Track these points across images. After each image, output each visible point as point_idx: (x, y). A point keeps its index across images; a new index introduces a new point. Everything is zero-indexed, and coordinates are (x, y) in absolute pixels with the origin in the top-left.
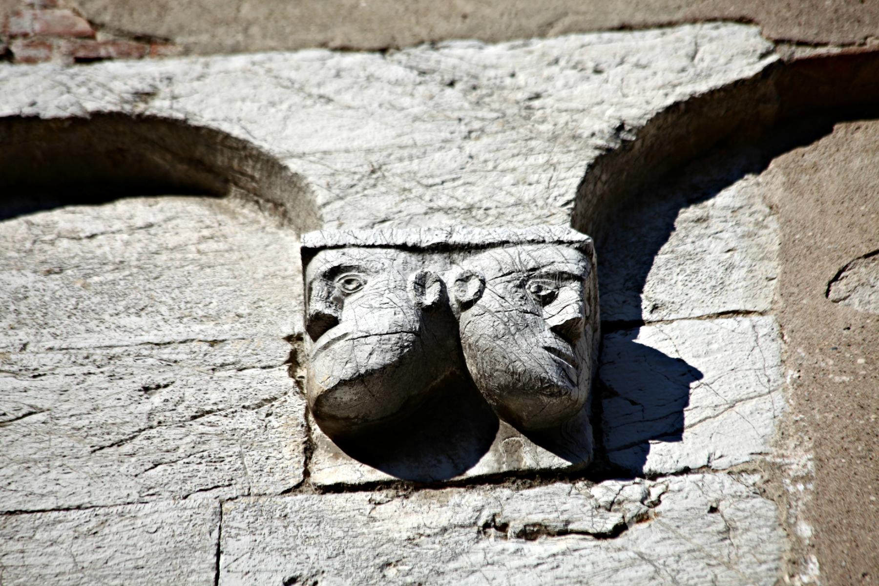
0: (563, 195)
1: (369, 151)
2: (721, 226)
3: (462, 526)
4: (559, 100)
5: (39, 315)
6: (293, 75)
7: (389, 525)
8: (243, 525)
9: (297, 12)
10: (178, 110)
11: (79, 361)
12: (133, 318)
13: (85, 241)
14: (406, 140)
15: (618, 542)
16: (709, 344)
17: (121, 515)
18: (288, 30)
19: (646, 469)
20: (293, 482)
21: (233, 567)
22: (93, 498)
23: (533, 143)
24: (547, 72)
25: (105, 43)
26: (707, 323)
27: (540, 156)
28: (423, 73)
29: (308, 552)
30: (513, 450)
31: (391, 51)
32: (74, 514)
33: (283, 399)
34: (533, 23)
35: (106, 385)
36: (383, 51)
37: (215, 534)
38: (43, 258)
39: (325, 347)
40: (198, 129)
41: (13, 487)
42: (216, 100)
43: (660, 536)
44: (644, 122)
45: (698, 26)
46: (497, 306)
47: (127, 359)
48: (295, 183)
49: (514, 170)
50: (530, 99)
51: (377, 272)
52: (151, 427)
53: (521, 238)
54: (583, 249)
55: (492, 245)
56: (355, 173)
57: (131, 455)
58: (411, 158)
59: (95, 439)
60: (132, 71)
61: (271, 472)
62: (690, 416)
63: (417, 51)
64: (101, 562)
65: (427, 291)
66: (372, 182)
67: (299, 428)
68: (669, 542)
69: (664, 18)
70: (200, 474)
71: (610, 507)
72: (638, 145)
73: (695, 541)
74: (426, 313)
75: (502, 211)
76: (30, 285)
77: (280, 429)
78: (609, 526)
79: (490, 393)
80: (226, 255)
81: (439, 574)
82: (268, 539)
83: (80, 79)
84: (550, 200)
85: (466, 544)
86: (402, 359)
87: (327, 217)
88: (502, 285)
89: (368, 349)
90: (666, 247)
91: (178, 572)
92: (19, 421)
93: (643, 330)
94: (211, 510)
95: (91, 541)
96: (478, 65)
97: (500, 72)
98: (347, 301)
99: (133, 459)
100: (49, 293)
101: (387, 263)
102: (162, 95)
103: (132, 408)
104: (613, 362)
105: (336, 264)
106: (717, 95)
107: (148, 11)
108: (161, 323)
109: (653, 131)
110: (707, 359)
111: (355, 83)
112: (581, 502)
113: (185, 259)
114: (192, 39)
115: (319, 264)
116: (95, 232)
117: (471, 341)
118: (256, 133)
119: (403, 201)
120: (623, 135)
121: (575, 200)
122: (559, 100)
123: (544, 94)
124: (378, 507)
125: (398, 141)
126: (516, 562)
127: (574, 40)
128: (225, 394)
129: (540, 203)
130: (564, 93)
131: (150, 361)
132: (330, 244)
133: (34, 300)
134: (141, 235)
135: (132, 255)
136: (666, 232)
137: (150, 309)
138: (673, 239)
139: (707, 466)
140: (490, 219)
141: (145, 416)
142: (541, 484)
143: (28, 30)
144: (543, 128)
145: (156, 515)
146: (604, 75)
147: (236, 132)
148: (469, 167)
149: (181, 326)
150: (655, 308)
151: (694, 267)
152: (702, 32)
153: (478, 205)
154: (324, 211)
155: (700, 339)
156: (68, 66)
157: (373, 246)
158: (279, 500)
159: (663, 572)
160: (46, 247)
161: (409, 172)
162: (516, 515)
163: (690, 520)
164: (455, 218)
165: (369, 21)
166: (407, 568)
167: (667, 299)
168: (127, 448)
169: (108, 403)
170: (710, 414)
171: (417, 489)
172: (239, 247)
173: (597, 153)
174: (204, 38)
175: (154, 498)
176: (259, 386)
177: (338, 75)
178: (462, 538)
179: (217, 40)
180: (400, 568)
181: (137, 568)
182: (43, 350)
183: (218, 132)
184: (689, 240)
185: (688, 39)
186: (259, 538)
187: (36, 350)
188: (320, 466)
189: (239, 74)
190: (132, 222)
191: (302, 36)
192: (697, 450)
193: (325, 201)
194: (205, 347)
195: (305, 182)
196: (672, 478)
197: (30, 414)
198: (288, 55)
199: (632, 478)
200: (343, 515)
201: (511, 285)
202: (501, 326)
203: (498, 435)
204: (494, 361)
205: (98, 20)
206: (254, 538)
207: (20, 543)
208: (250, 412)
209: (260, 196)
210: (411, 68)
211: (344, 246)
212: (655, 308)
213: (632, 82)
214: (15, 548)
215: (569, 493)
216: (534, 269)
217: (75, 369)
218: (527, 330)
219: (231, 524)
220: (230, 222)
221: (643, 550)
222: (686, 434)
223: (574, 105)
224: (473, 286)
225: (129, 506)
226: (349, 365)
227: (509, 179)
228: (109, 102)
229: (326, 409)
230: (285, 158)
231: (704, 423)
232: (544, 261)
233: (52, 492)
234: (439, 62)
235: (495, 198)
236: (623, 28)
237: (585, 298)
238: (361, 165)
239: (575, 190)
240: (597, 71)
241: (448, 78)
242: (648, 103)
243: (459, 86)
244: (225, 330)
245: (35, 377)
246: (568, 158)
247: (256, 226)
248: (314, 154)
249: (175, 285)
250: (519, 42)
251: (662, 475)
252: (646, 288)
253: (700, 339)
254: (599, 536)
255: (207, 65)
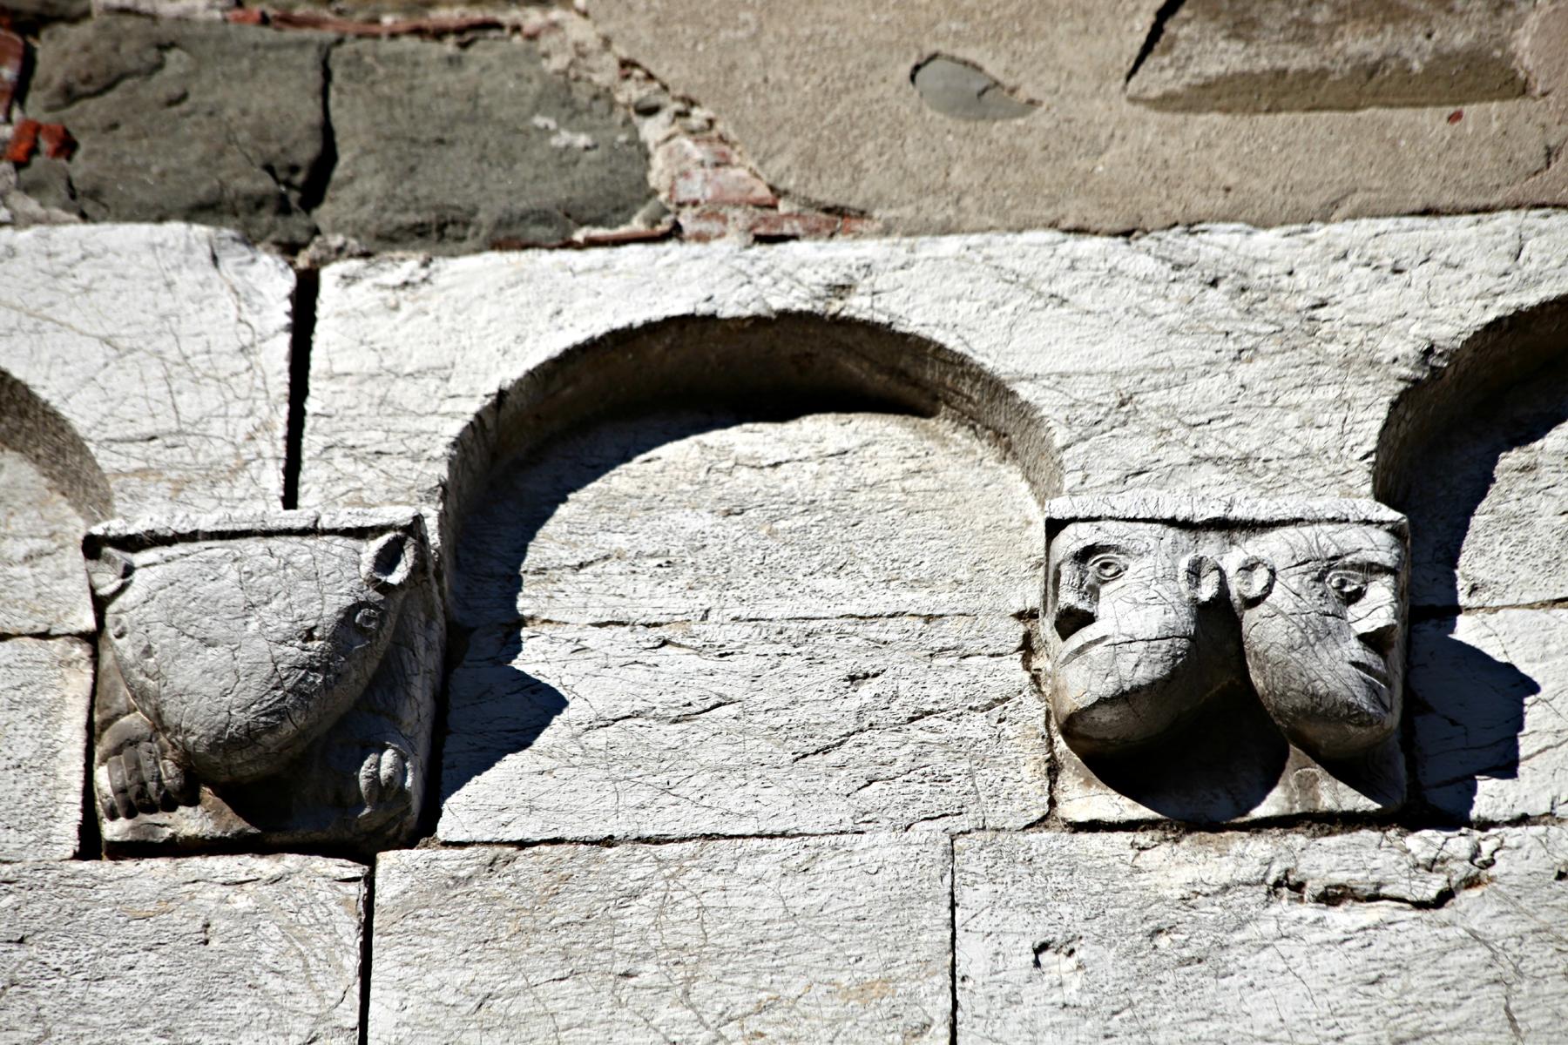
0: (1361, 444)
1: (1116, 374)
2: (1554, 478)
3: (1247, 884)
4: (1349, 310)
5: (720, 571)
6: (1018, 265)
7: (1157, 878)
8: (981, 871)
9: (1019, 178)
10: (879, 311)
11: (772, 638)
12: (831, 579)
13: (768, 471)
14: (1161, 361)
15: (1444, 913)
16: (1545, 644)
17: (835, 848)
18: (1009, 202)
19: (1474, 814)
20: (1036, 815)
21: (972, 925)
22: (799, 823)
23: (1321, 370)
24: (1334, 270)
25: (789, 215)
26: (1541, 615)
27: (1331, 388)
28: (1178, 267)
29: (1060, 910)
30: (1307, 785)
31: (1136, 234)
32: (779, 843)
33: (1017, 699)
34: (1315, 202)
35: (805, 671)
36: (1127, 234)
37: (947, 880)
38: (720, 494)
39: (1080, 651)
40: (905, 336)
41: (706, 802)
42: (925, 298)
43: (1496, 908)
44: (1458, 344)
45: (1523, 212)
46: (1292, 606)
47: (825, 636)
48: (1025, 413)
49: (1298, 406)
50: (1314, 307)
51: (1141, 555)
52: (861, 731)
53: (1319, 514)
54: (1395, 531)
55: (1282, 523)
56: (1100, 405)
57: (842, 767)
58: (1168, 386)
59: (796, 743)
60: (823, 255)
61: (1009, 799)
62: (1526, 745)
63: (1169, 236)
64: (816, 909)
65: (1203, 581)
66: (1122, 418)
67: (1039, 741)
68: (1509, 917)
69: (1480, 201)
70: (923, 798)
71: (1431, 866)
72: (1451, 369)
73: (1541, 917)
74: (1203, 611)
75: (1285, 464)
76: (707, 530)
77: (1017, 741)
78: (1432, 894)
79: (1280, 713)
80: (937, 496)
81: (1223, 947)
82: (1012, 890)
83: (762, 265)
84: (1345, 451)
85: (1253, 909)
86: (1174, 671)
87: (1069, 466)
88: (1296, 578)
89: (1133, 658)
90: (1484, 505)
91: (907, 928)
92: (706, 714)
93: (1462, 621)
94: (940, 848)
95: (802, 881)
96: (1246, 257)
97: (1275, 269)
98: (1104, 590)
99: (843, 773)
100: (730, 541)
101: (1153, 543)
102: (860, 290)
103: (837, 704)
104: (1425, 665)
105: (1090, 543)
106: (1548, 309)
107: (840, 175)
108: (864, 588)
109: (1468, 354)
110: (1543, 665)
111: (1095, 277)
112: (1395, 857)
113: (888, 501)
114: (893, 213)
115: (1069, 542)
116: (778, 459)
117: (1259, 648)
118: (975, 345)
119: (1161, 445)
120: (1432, 360)
121: (1375, 451)
122: (1349, 310)
123: (1332, 301)
124: (1143, 853)
125: (1151, 361)
126: (1317, 936)
127: (1366, 227)
128: (947, 690)
129: (1333, 454)
130: (1356, 301)
131: (855, 641)
132: (1081, 515)
133: (713, 551)
134: (832, 466)
135: (825, 490)
136: (1483, 483)
137: (850, 568)
138: (1493, 495)
139: (1550, 814)
140: (1271, 475)
141: (853, 716)
142: (1341, 832)
143: (698, 195)
144: (1332, 348)
145: (876, 850)
146: (1405, 277)
147: (952, 343)
148: (1241, 403)
149: (889, 593)
150: (1474, 589)
151: (1521, 533)
152: (1528, 222)
153: (1255, 455)
154: (1066, 455)
155: (1534, 637)
156: (748, 247)
157: (1134, 520)
158: (1020, 837)
159: (1502, 958)
160: (723, 478)
161: (1167, 405)
162: (1314, 872)
163: (1533, 889)
164: (1227, 472)
165: (1109, 193)
166: (1183, 937)
167: (1488, 578)
168: (834, 757)
169: (810, 695)
170: (1551, 743)
171: (1189, 831)
172: (952, 486)
173: (1402, 386)
174: (908, 211)
175: (871, 826)
176: (988, 681)
177: (1072, 268)
178: (1249, 900)
179: (923, 215)
180: (1175, 937)
181: (857, 919)
182: (727, 620)
183: (930, 342)
184: (1514, 496)
185: (1510, 231)
186: (1001, 888)
187: (719, 619)
188: (1068, 795)
189: (952, 262)
190: (822, 446)
191: (1026, 211)
192: (1537, 792)
193: (1064, 443)
194: (919, 624)
195: (1039, 414)
196: (1507, 829)
197: (719, 705)
198: (1010, 237)
199: (1457, 828)
200: (1100, 863)
201: (1308, 578)
202: (1298, 634)
203: (1289, 764)
204: (1288, 679)
205: (781, 186)
206: (994, 888)
207: (721, 877)
208: (979, 715)
209: (979, 421)
210: (1164, 260)
211: (1098, 519)
212: (1474, 589)
213: (1442, 286)
214: (715, 884)
215: (1379, 846)
216: (1335, 558)
217: (766, 648)
218: (1330, 639)
219: (966, 867)
220: (940, 452)
221: (1476, 928)
222: (1521, 769)
223: (1369, 318)
224: (1260, 579)
225: (843, 837)
226: (1110, 679)
227: (1292, 419)
228: (798, 298)
229: (1079, 729)
230: (1012, 381)
231: (1544, 755)
232: (1348, 548)
233: (751, 812)
234: (1197, 252)
235: (1275, 445)
236: (1427, 212)
237: (1400, 594)
238: (1107, 394)
239: (1376, 438)
240: (1397, 271)
241: (1209, 275)
242: (1462, 318)
243: (1223, 286)
244: (943, 600)
245: (721, 656)
246: (1365, 392)
247: (971, 458)
248: (1048, 377)
249: (878, 536)
250: (1298, 227)
251: (1494, 824)
252: (1462, 561)
253: (1534, 637)
254: (1420, 905)
255: (912, 250)
